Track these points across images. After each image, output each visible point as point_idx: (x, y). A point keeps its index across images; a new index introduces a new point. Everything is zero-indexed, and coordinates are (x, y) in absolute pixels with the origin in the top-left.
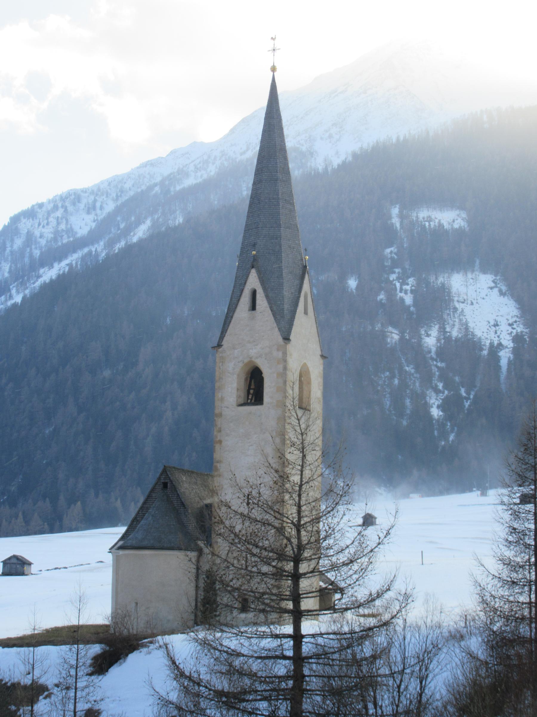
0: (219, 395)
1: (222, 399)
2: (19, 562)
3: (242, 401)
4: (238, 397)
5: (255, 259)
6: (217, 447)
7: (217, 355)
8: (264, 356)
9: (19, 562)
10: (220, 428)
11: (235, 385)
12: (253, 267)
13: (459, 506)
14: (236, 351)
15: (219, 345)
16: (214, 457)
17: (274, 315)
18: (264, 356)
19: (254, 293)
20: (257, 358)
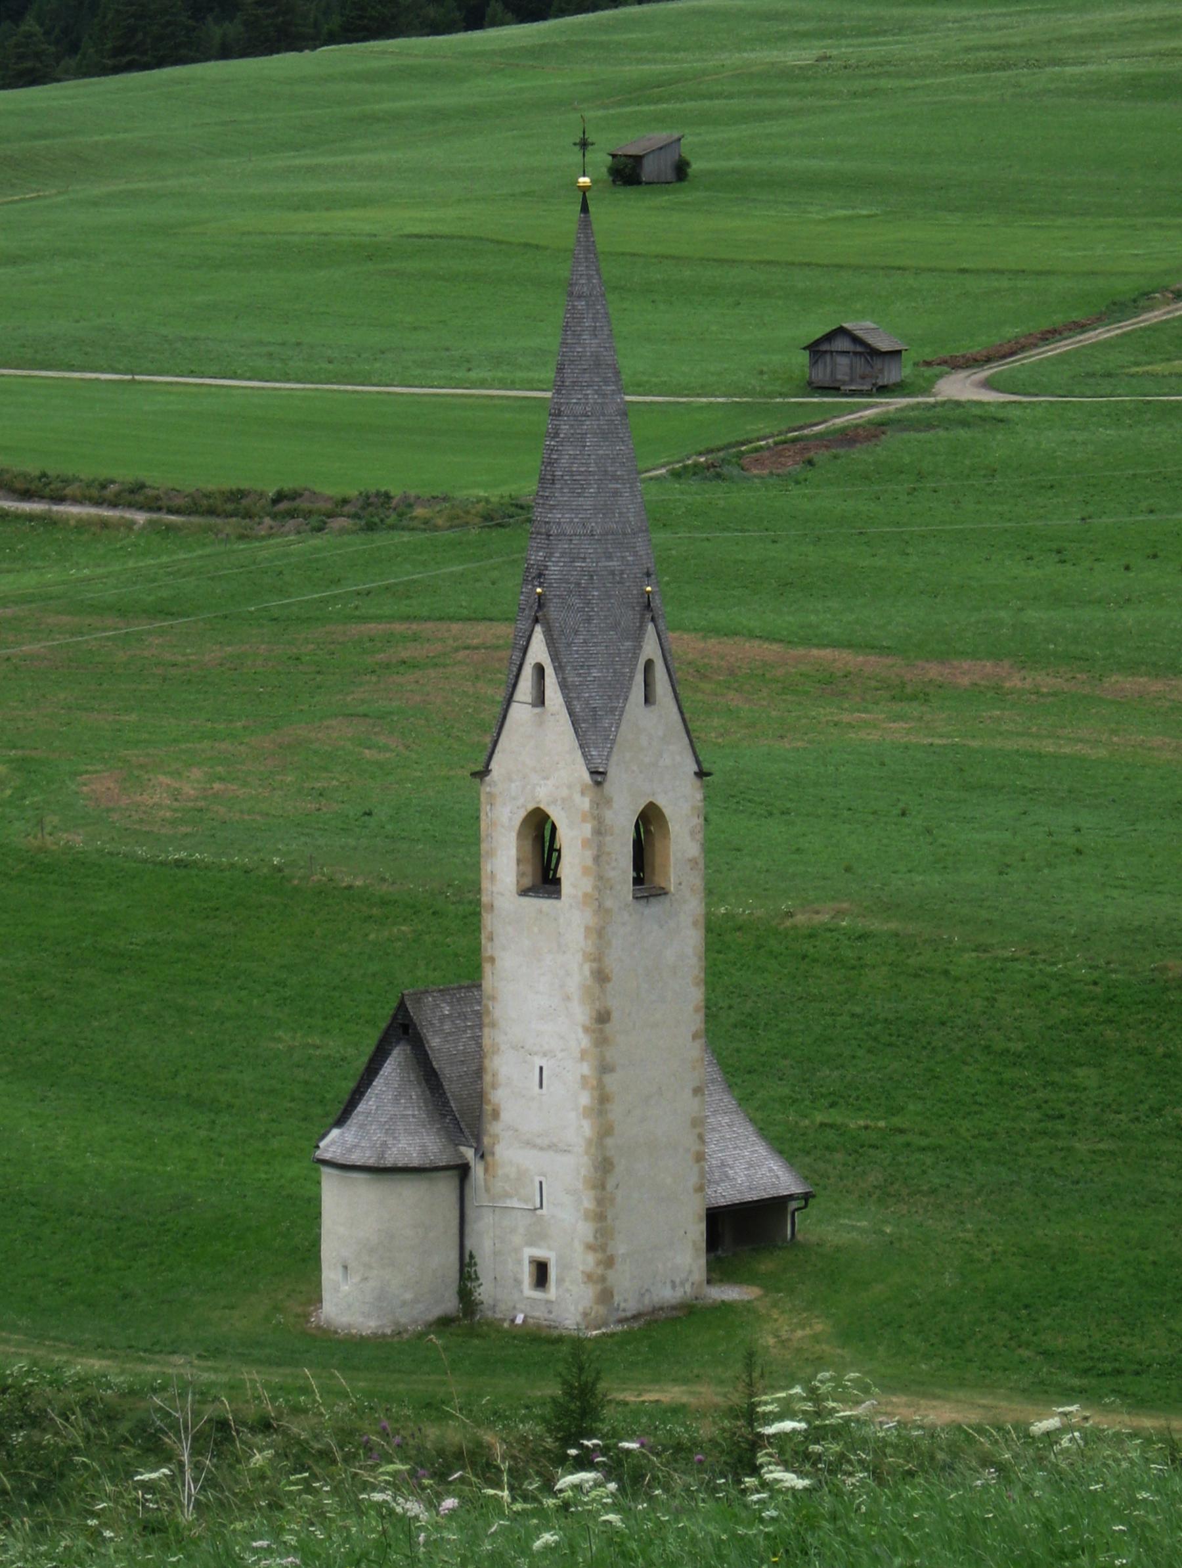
0: (487, 867)
1: (492, 876)
2: (859, 349)
3: (527, 882)
4: (521, 875)
5: (541, 601)
6: (487, 967)
7: (482, 789)
8: (559, 802)
9: (859, 349)
10: (492, 933)
11: (512, 852)
12: (536, 620)
13: (541, 1086)
14: (513, 785)
15: (486, 771)
16: (703, 989)
17: (574, 723)
18: (559, 802)
19: (540, 670)
20: (548, 805)
